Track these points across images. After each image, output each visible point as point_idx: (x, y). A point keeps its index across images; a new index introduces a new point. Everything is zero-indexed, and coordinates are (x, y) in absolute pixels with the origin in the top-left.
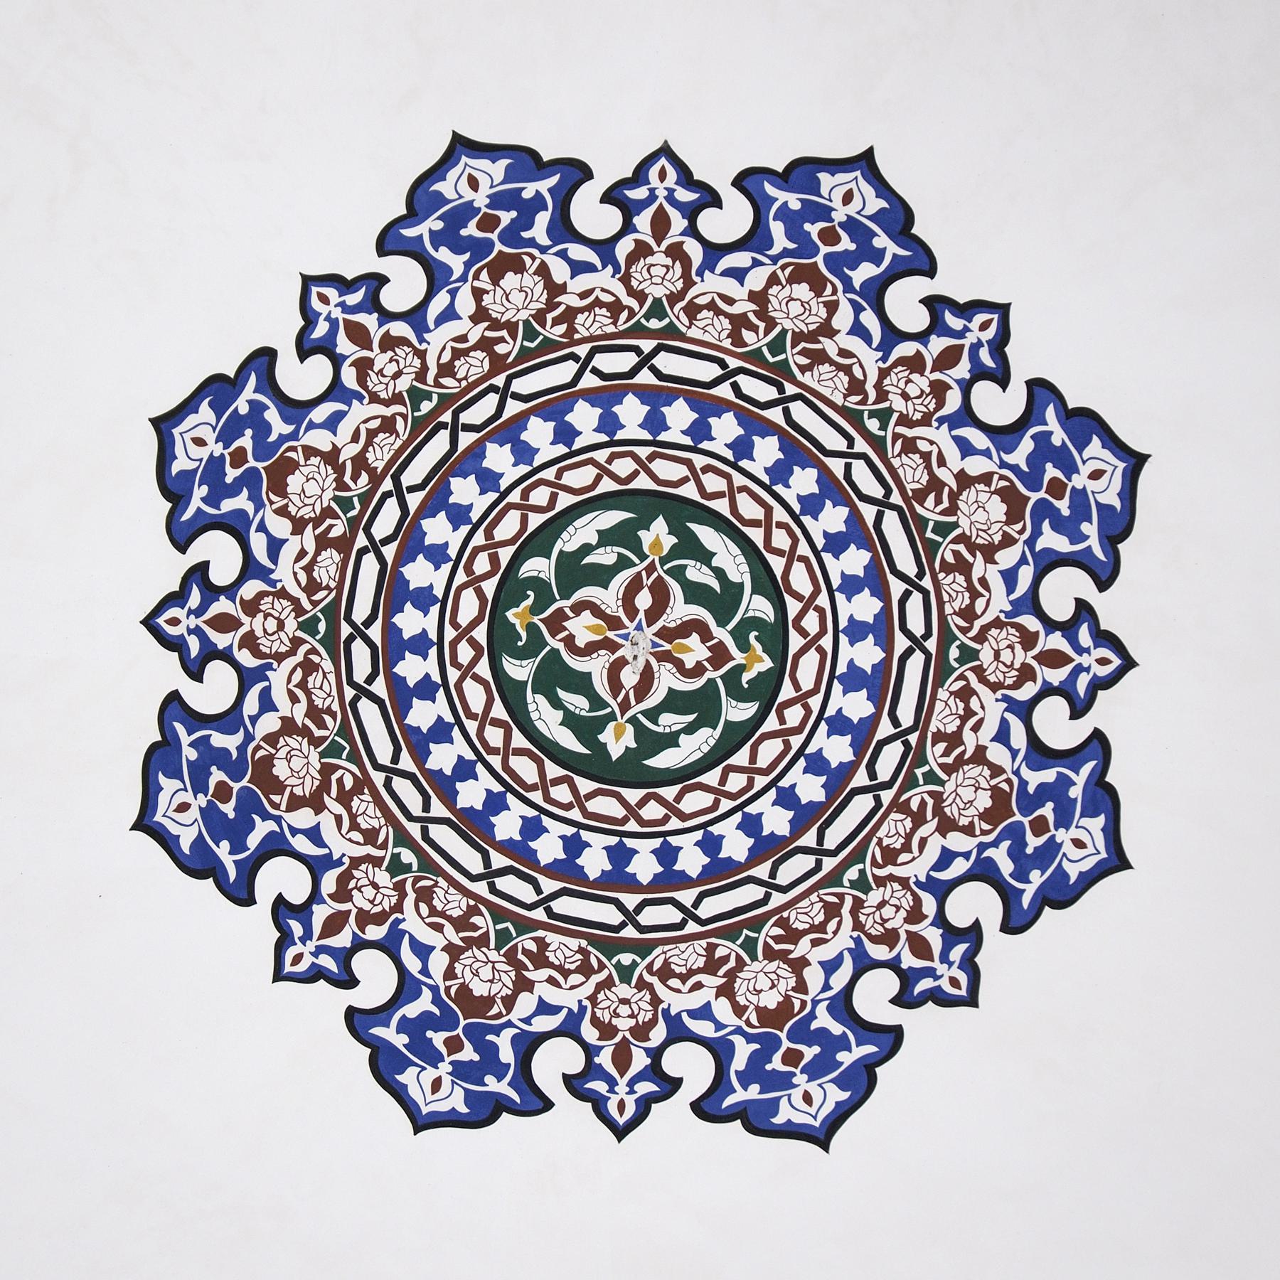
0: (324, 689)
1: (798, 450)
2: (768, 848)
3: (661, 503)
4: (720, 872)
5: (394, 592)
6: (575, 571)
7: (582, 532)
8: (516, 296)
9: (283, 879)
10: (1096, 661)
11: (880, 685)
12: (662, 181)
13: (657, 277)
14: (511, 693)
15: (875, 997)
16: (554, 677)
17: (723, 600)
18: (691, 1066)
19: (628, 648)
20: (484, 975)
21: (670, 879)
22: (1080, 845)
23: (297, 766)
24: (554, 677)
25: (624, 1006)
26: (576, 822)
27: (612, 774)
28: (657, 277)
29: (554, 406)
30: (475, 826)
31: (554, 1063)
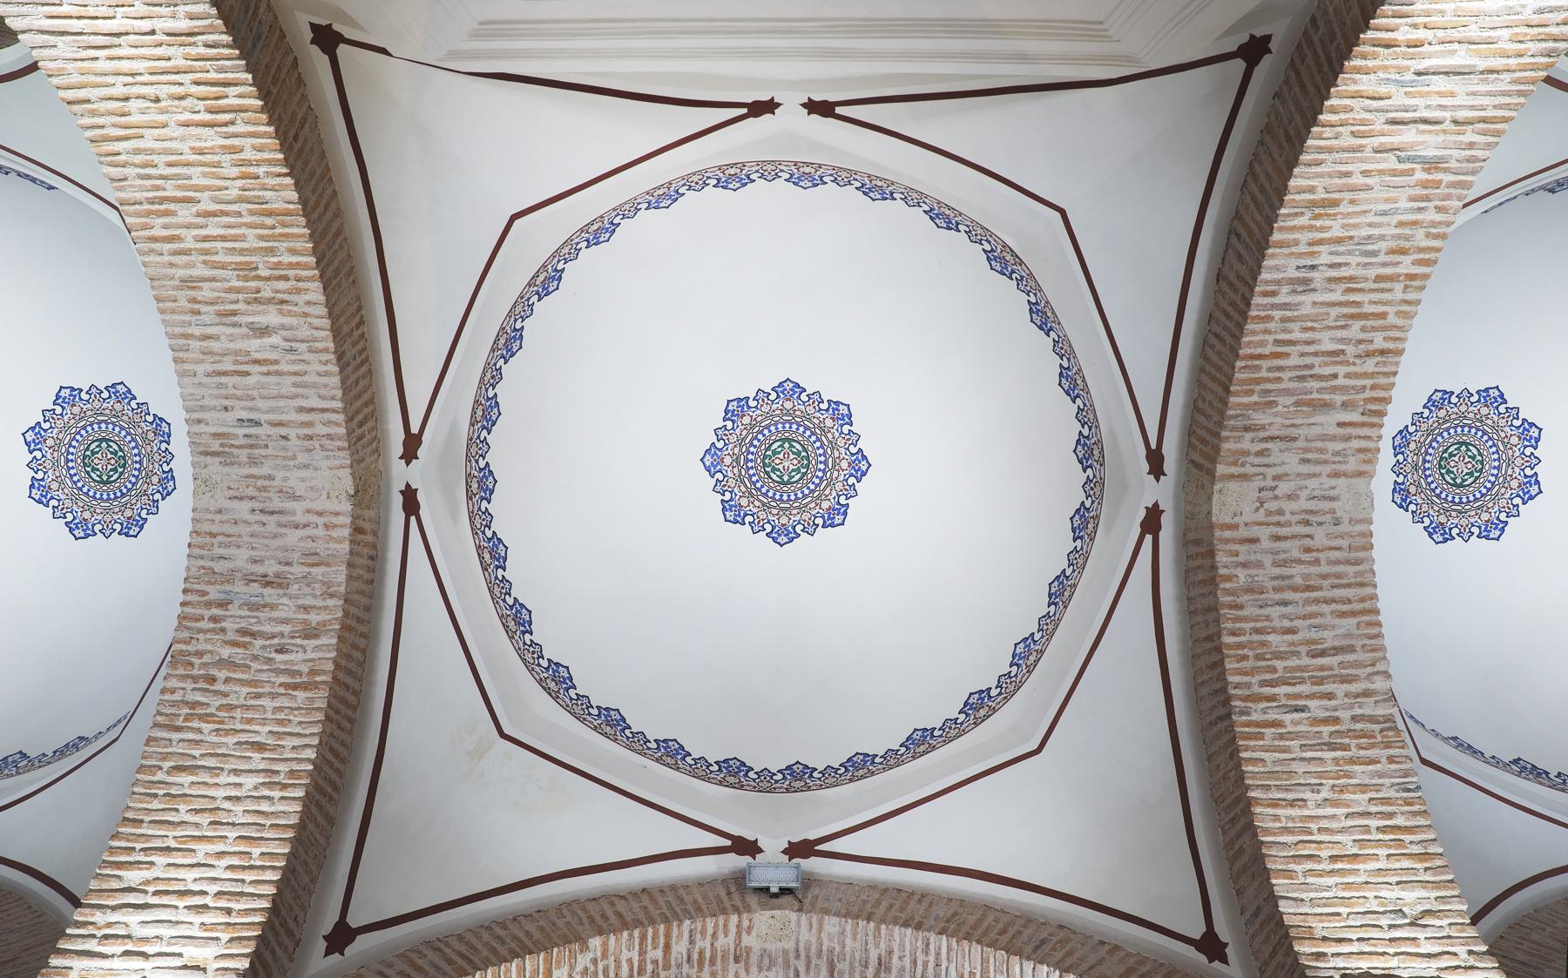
0: (736, 450)
1: (1485, 433)
2: (1483, 495)
3: (1464, 443)
4: (1476, 500)
5: (1425, 461)
6: (1451, 455)
7: (775, 446)
8: (1442, 413)
9: (1412, 507)
10: (1534, 461)
11: (1498, 468)
12: (854, 438)
13: (1463, 408)
14: (805, 450)
15: (1503, 517)
16: (1449, 472)
17: (1473, 457)
18: (1475, 530)
19: (1461, 467)
20: (1443, 519)
21: (749, 452)
22: (1534, 490)
23: (1413, 489)
24: (1449, 472)
25: (1464, 522)
26: (1453, 494)
27: (1458, 486)
28: (1463, 408)
29: (1447, 430)
30: (1438, 496)
31: (1455, 532)
